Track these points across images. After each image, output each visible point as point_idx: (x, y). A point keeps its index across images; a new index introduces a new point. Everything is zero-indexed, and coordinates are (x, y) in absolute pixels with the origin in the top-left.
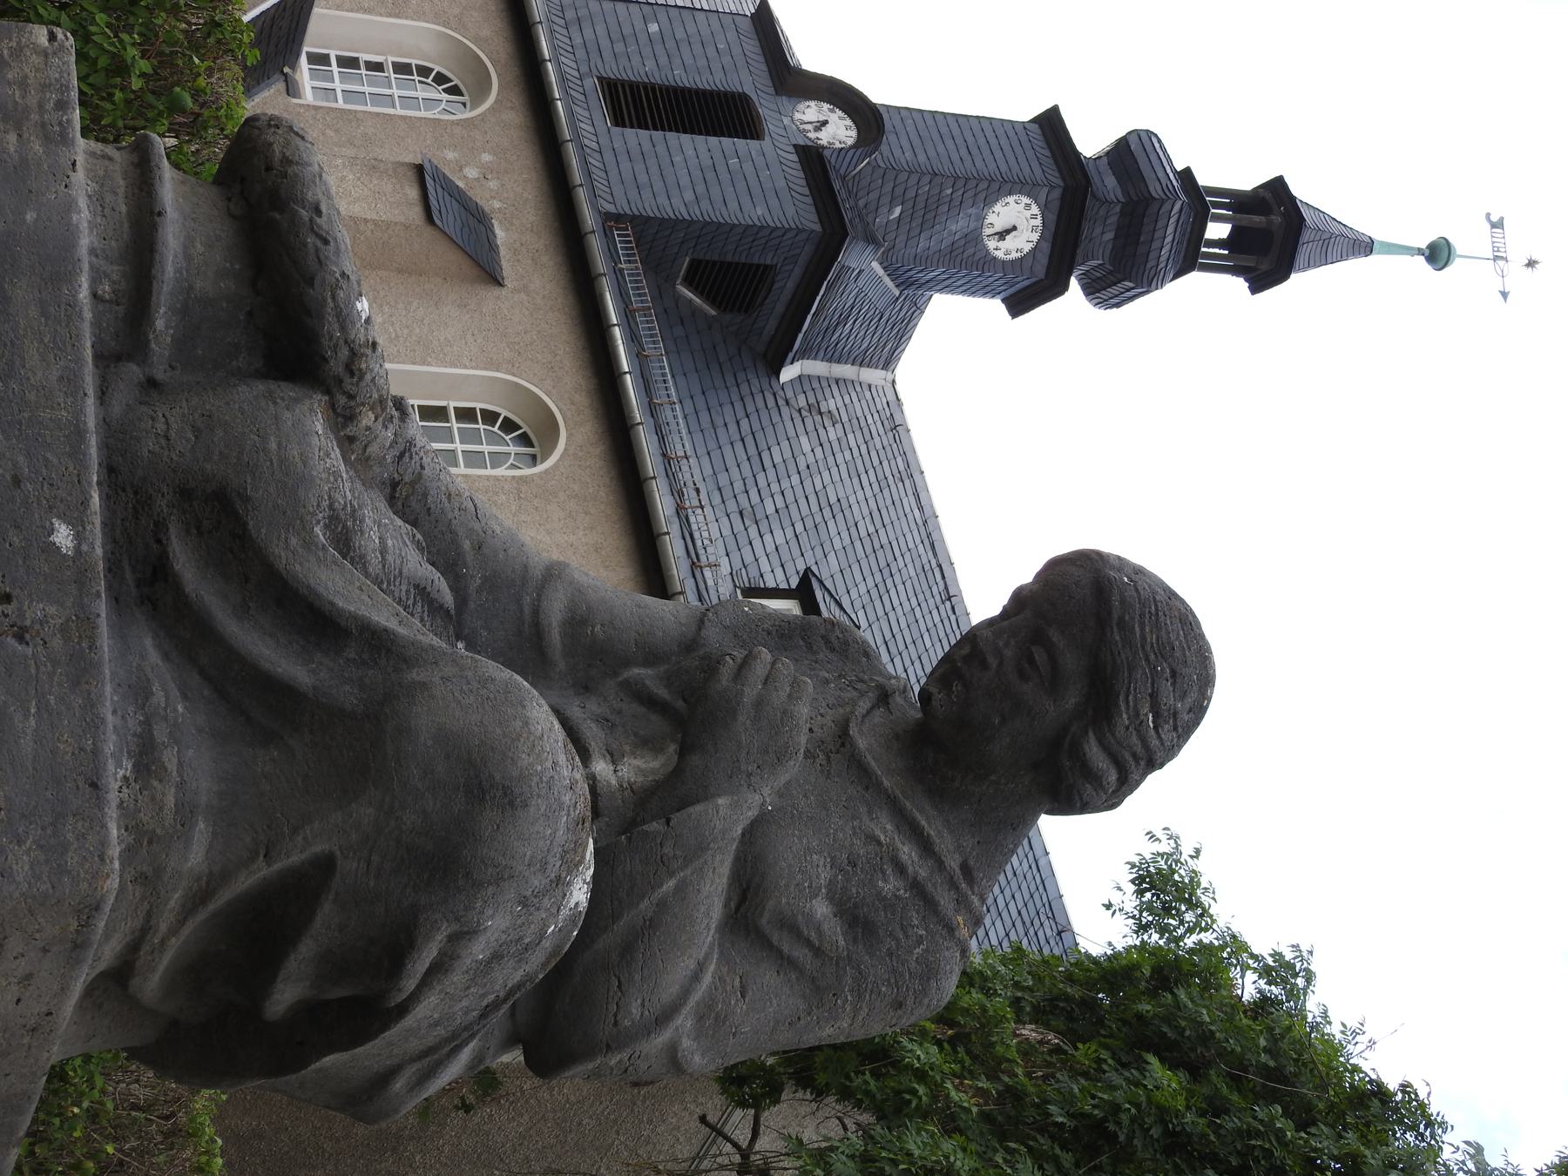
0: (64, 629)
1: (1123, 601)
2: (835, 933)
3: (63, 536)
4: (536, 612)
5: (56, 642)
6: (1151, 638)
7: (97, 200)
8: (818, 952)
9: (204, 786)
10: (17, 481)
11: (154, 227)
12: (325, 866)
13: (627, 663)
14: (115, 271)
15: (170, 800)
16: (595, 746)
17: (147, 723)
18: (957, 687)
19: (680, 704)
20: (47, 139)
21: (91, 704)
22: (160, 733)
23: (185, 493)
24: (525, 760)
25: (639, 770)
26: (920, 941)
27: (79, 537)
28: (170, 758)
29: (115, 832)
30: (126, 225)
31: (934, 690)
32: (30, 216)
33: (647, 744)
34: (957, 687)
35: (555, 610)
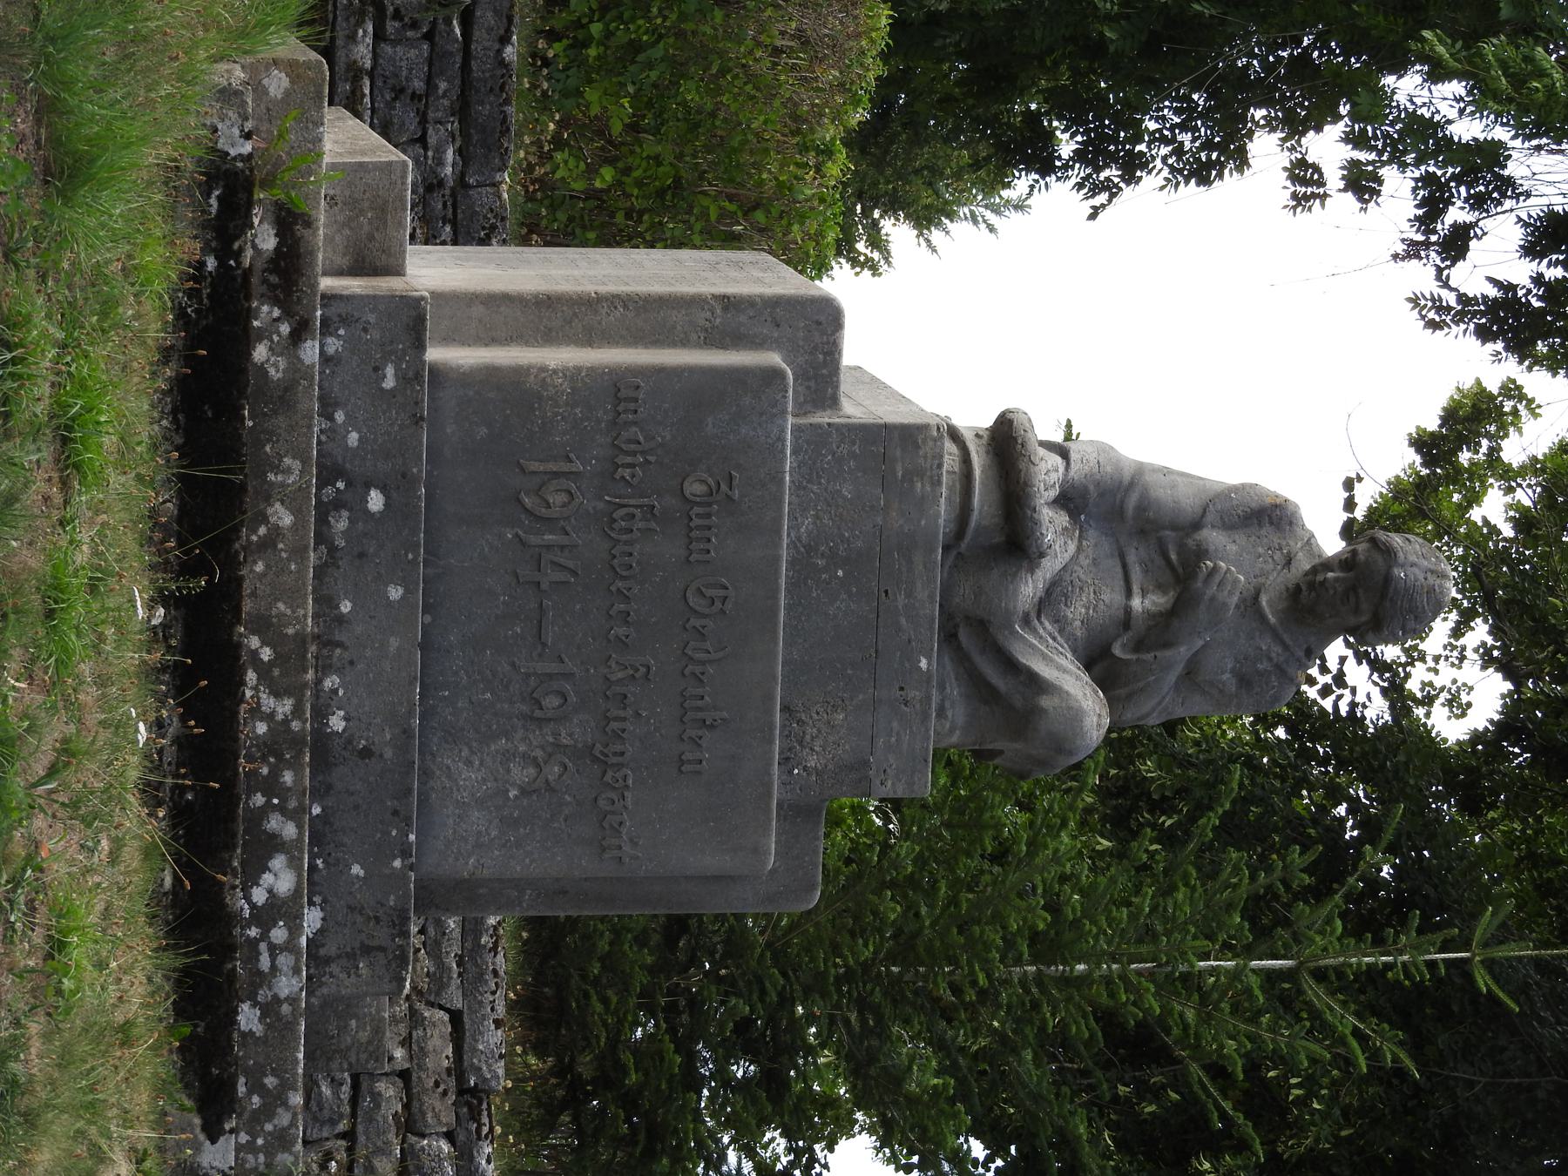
0: (921, 701)
1: (1396, 588)
2: (1232, 686)
3: (923, 664)
4: (1122, 502)
5: (918, 706)
6: (1406, 605)
7: (949, 499)
8: (1221, 691)
9: (961, 720)
10: (909, 641)
11: (969, 515)
12: (1001, 752)
13: (1164, 528)
14: (952, 525)
15: (948, 726)
16: (1136, 588)
17: (943, 700)
18: (1313, 594)
19: (1180, 570)
20: (933, 484)
21: (927, 730)
22: (947, 704)
23: (967, 618)
24: (1078, 742)
25: (1154, 603)
26: (1274, 687)
27: (929, 664)
28: (949, 714)
29: (944, 889)
30: (958, 486)
31: (1304, 588)
32: (923, 522)
33: (1161, 588)
34: (1313, 594)
35: (1132, 501)
